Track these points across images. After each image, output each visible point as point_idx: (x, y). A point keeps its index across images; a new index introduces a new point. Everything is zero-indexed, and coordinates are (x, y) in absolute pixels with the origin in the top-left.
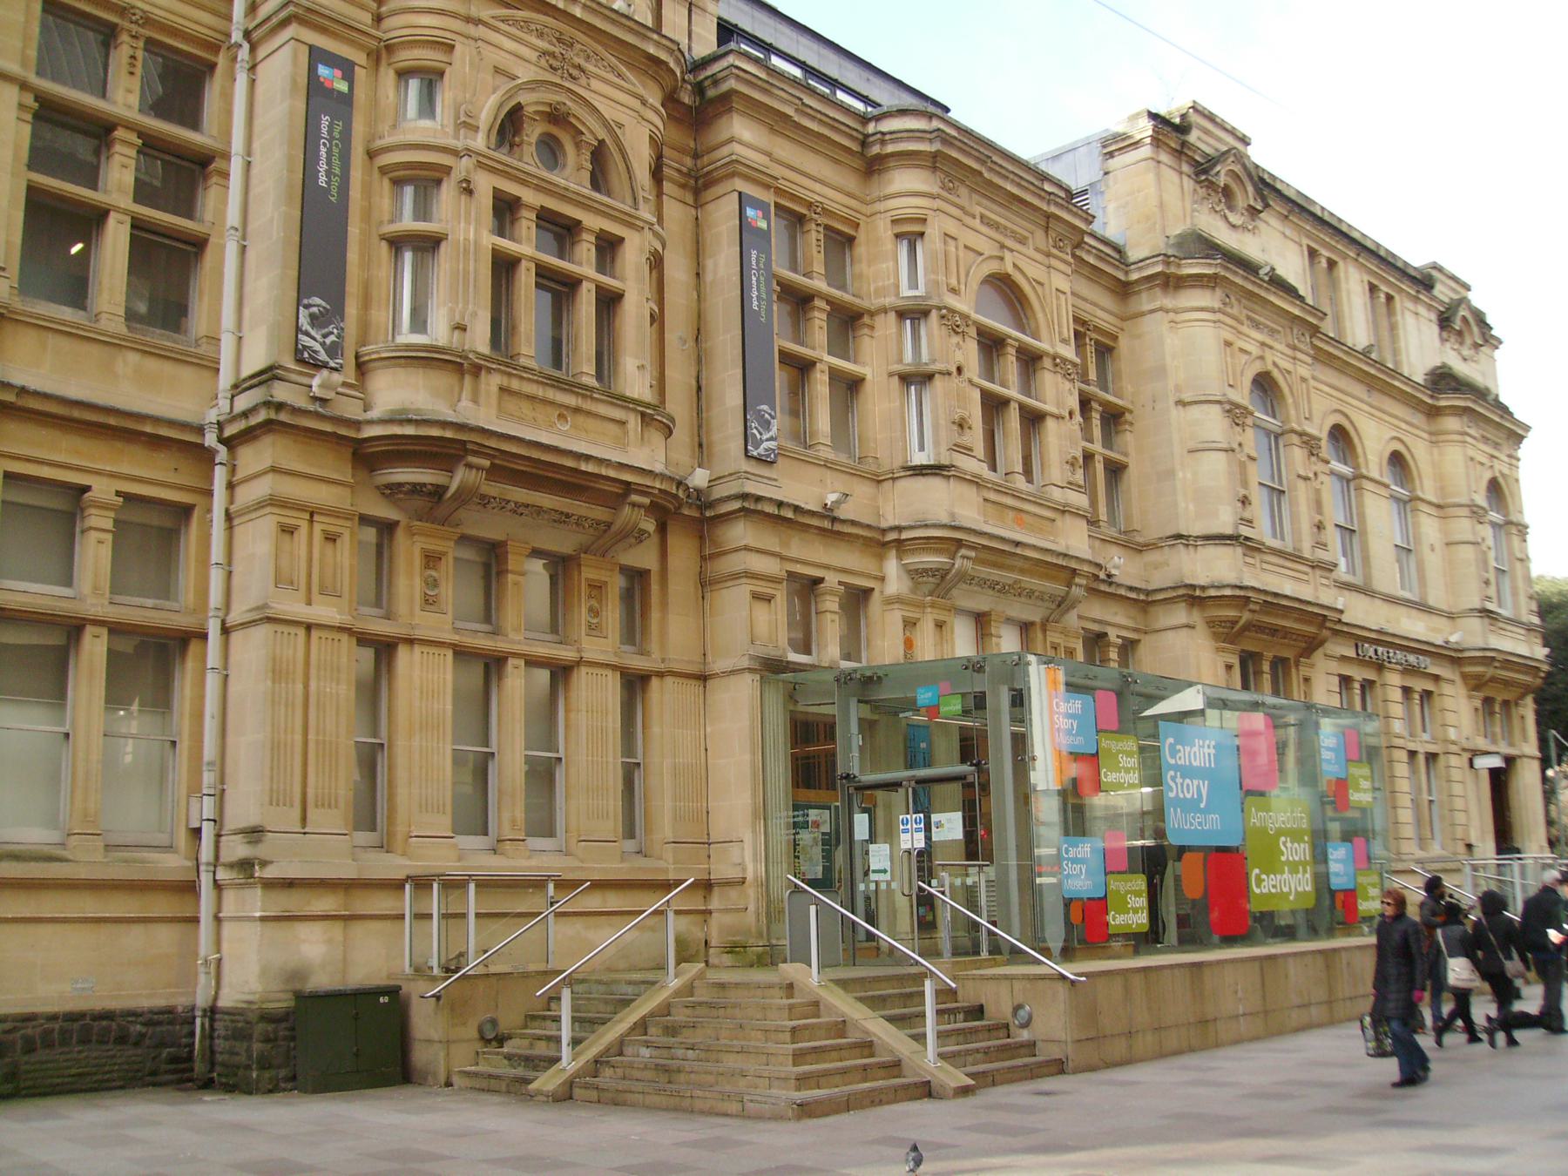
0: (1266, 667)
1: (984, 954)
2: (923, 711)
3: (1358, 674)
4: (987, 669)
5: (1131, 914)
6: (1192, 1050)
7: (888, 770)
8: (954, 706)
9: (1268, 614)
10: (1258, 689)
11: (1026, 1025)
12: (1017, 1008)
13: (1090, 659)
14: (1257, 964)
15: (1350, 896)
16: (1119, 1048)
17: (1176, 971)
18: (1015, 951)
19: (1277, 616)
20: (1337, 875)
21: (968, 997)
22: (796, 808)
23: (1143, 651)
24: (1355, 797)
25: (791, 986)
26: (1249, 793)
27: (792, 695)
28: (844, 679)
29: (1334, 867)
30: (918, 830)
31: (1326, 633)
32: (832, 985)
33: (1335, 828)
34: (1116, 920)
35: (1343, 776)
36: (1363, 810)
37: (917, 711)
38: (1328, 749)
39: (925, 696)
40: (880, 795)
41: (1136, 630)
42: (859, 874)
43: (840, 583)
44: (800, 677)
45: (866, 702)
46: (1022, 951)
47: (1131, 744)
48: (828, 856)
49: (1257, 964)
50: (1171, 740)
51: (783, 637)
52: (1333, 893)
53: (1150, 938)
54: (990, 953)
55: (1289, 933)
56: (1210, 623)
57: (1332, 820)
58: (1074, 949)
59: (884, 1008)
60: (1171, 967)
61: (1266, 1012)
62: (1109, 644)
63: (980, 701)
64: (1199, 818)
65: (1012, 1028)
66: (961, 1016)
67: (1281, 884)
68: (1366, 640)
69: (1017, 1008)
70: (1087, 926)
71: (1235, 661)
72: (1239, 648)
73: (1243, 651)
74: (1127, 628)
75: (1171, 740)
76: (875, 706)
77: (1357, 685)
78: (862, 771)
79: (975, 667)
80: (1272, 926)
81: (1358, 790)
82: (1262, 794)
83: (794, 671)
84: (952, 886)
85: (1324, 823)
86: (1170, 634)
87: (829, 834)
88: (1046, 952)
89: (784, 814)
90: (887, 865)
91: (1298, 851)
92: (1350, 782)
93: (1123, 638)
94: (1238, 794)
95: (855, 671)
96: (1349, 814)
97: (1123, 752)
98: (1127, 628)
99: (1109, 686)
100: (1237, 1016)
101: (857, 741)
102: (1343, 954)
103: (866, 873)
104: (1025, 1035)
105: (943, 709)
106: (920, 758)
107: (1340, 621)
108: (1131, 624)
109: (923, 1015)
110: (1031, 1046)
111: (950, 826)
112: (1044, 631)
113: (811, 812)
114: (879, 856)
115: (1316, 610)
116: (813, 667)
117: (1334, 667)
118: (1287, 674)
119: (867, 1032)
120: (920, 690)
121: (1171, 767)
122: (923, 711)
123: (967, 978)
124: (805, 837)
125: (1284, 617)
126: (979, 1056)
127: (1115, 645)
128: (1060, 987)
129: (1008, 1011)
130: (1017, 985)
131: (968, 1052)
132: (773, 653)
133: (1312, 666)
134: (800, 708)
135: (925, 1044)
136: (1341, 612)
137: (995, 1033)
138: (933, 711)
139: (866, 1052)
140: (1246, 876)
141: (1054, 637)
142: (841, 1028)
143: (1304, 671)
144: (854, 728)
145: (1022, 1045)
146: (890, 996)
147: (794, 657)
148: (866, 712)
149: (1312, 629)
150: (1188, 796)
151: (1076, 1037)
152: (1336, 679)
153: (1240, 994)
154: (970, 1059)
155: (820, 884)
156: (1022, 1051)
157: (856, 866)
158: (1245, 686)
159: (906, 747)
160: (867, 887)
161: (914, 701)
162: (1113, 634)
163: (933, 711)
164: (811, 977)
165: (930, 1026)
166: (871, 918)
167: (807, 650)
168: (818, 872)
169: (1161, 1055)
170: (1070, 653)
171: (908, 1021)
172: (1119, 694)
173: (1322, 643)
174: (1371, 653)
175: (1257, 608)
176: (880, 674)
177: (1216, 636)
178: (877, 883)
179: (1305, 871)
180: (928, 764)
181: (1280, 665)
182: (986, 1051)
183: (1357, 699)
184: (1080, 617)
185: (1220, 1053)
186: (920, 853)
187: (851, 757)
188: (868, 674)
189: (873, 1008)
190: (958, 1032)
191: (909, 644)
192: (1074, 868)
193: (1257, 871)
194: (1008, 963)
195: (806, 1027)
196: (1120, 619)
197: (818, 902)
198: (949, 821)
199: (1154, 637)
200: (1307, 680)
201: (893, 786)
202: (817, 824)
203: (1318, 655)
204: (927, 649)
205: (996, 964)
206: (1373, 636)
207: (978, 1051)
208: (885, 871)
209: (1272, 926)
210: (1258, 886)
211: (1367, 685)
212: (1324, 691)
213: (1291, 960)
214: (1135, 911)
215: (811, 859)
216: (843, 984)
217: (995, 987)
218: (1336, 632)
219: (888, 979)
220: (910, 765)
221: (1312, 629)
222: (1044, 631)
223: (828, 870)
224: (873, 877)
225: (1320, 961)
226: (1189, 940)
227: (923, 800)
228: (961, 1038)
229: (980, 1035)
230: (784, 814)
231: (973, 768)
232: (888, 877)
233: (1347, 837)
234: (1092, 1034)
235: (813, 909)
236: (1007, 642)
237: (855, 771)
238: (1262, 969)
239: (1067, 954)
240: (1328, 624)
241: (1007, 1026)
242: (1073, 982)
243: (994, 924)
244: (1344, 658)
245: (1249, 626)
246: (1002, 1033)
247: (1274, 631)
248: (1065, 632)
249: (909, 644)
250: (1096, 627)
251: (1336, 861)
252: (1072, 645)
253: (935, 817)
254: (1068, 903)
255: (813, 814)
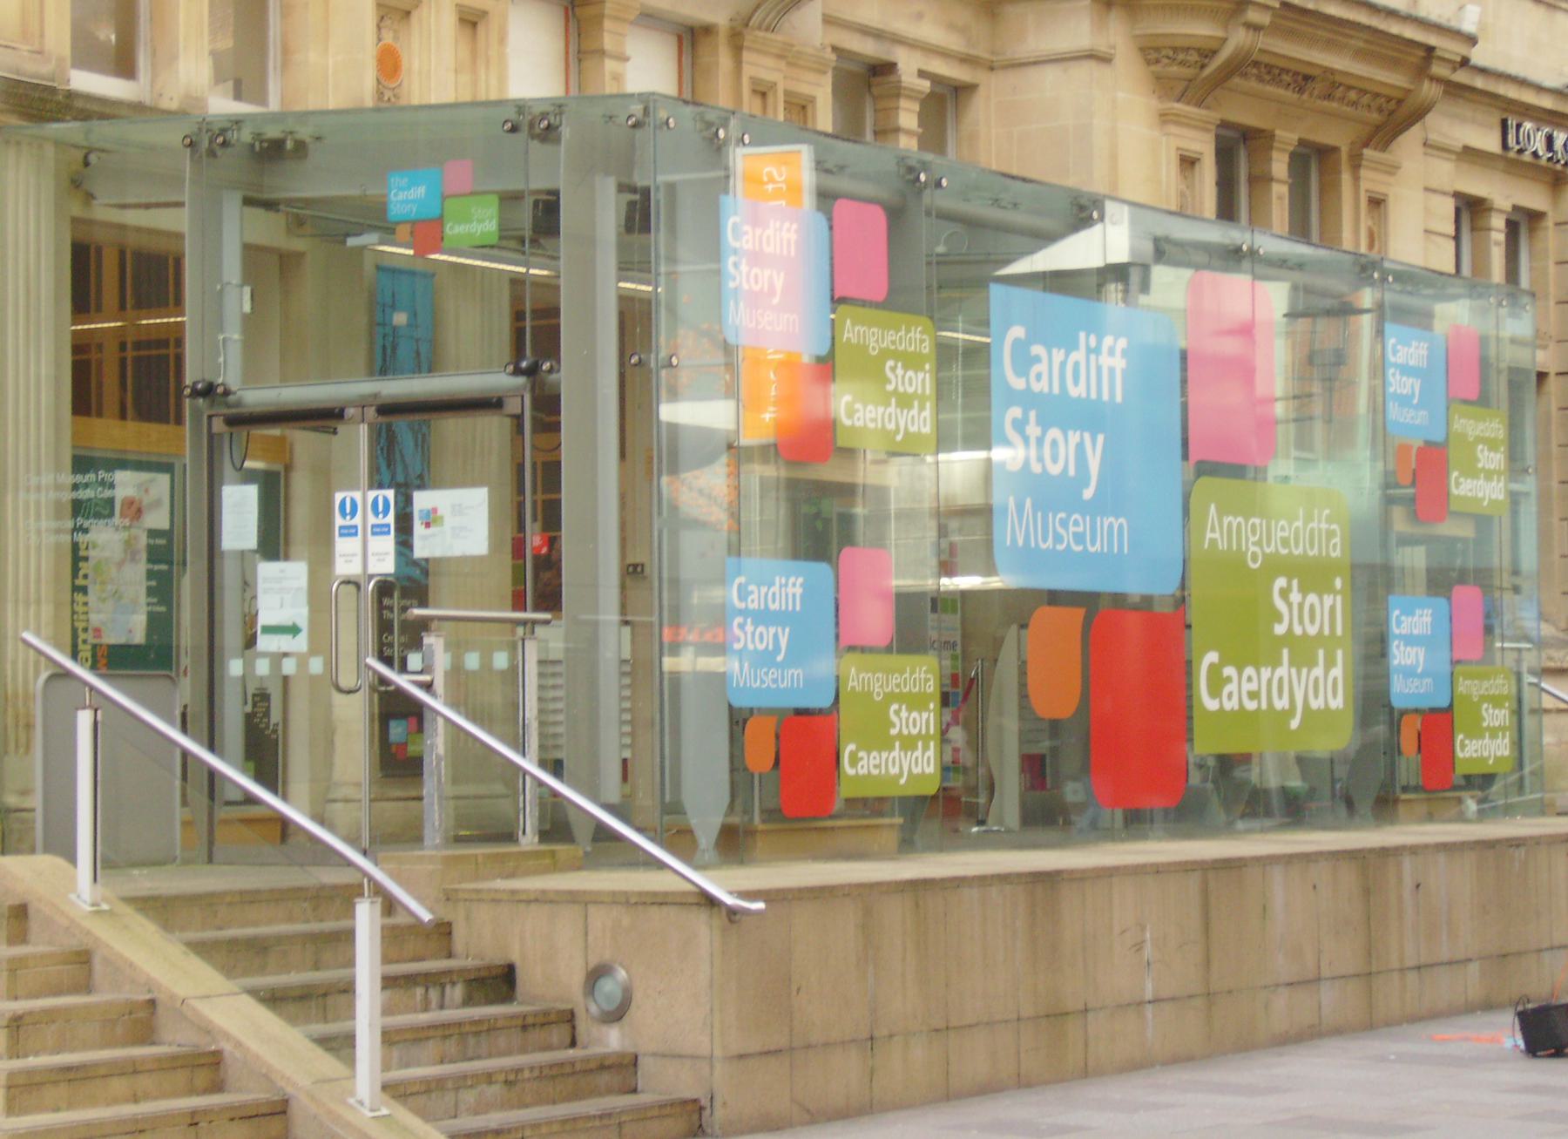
0: (1279, 166)
1: (529, 840)
2: (403, 232)
3: (1503, 193)
4: (566, 132)
5: (900, 749)
6: (1023, 1083)
7: (326, 376)
8: (483, 222)
9: (1290, 34)
10: (1259, 220)
11: (617, 1015)
12: (597, 974)
13: (850, 129)
14: (1194, 881)
15: (1438, 726)
16: (843, 1075)
17: (994, 891)
18: (603, 834)
19: (1313, 41)
20: (1409, 672)
21: (479, 943)
22: (82, 464)
23: (983, 113)
24: (1463, 487)
25: (20, 912)
26: (1206, 469)
27: (78, 180)
28: (210, 142)
29: (1402, 656)
30: (379, 530)
31: (1429, 90)
32: (128, 910)
33: (1415, 559)
34: (866, 766)
35: (1438, 436)
36: (1483, 521)
37: (388, 230)
38: (1405, 370)
39: (407, 196)
40: (303, 440)
41: (966, 60)
42: (231, 635)
43: (922, 74)
44: (103, 132)
45: (270, 205)
46: (617, 837)
47: (916, 337)
48: (162, 588)
49: (1194, 881)
50: (1017, 332)
51: (58, 37)
52: (1395, 718)
53: (949, 808)
54: (545, 836)
55: (1293, 810)
56: (1152, 52)
57: (1405, 541)
58: (751, 833)
59: (262, 970)
60: (983, 881)
61: (1209, 995)
62: (897, 92)
63: (547, 213)
64: (1079, 523)
65: (582, 1026)
66: (457, 992)
67: (1276, 692)
68: (1528, 111)
69: (597, 974)
70: (790, 774)
71: (1204, 147)
72: (1215, 116)
73: (1224, 124)
74: (944, 54)
75: (1017, 332)
76: (301, 216)
77: (1498, 222)
78: (252, 375)
79: (537, 126)
80: (1235, 791)
81: (1471, 472)
82: (1236, 471)
83: (84, 116)
84: (456, 672)
85: (1384, 545)
86: (1051, 74)
87: (167, 534)
88: (679, 839)
89: (47, 479)
90: (299, 613)
91: (1320, 613)
92: (1452, 454)
93: (935, 79)
94: (1174, 471)
95: (238, 122)
96: (1448, 529)
97: (897, 355)
98: (944, 54)
99: (868, 189)
100: (1140, 1004)
101: (240, 301)
102: (1407, 863)
103: (251, 642)
104: (613, 1040)
105: (453, 230)
106: (404, 352)
107: (1465, 62)
108: (954, 42)
109: (348, 989)
110: (625, 1068)
111: (461, 522)
112: (737, 47)
113: (121, 476)
114: (281, 591)
115: (1409, 32)
116: (138, 109)
117: (1449, 175)
118: (1330, 188)
119: (208, 1030)
120: (396, 180)
121: (1013, 397)
122: (403, 232)
123: (478, 897)
124: (105, 538)
125: (1330, 45)
126: (495, 1090)
127: (912, 94)
128: (702, 925)
129: (575, 979)
130: (599, 918)
131: (462, 1082)
132: (33, 69)
133: (1392, 169)
134: (102, 212)
135: (351, 1062)
136: (1472, 40)
137: (536, 1036)
138: (428, 232)
139: (202, 1078)
140: (1188, 669)
141: (759, 66)
142: (144, 1018)
143: (1371, 180)
144: (232, 265)
145: (604, 1065)
146: (280, 939)
147: (87, 82)
148: (267, 229)
149: (1396, 79)
150: (1055, 470)
151: (735, 1049)
152: (1449, 206)
153: (1148, 951)
154: (469, 1097)
155: (117, 660)
156: (604, 1079)
157: (224, 618)
158: (1227, 211)
159: (372, 324)
160: (249, 666)
161: (381, 208)
162: (909, 66)
163: (428, 232)
164: (72, 888)
165: (367, 1011)
166: (264, 754)
167: (124, 66)
168: (133, 627)
169: (948, 1094)
170: (800, 107)
171: (316, 1002)
172: (896, 215)
173: (1418, 115)
174: (1539, 144)
175: (1264, 18)
176: (304, 133)
177: (1162, 86)
178: (278, 658)
179: (1330, 663)
180: (428, 363)
181: (1314, 161)
182: (511, 1080)
183: (1497, 256)
184: (829, 20)
185: (1093, 1091)
186: (385, 588)
187: (220, 339)
188: (273, 132)
189: (229, 971)
190: (444, 1030)
191: (389, 64)
192: (755, 630)
193: (1212, 657)
194: (589, 862)
195: (50, 1015)
196: (931, 31)
197: (100, 703)
198: (458, 510)
199: (1012, 77)
200: (1377, 203)
201: (325, 417)
202: (135, 510)
203: (1410, 141)
204: (436, 74)
205: (556, 867)
206: (1547, 102)
207: (489, 1077)
208: (293, 630)
209: (1235, 791)
210: (1215, 692)
211: (1522, 223)
212: (1417, 231)
213: (1277, 873)
214: (909, 743)
215: (117, 596)
216: (160, 908)
217: (545, 927)
218: (1456, 91)
219: (280, 896)
220: (384, 366)
221: (1396, 79)
222: (737, 47)
223: (161, 625)
224: (265, 643)
225: (1349, 876)
226: (1045, 816)
227: (405, 446)
228: (451, 1046)
229: (502, 1041)
230: (47, 479)
231: (520, 373)
232: (300, 643)
233: (1440, 582)
234: (780, 1040)
235: (84, 719)
236: (643, 68)
237: (230, 374)
238: (1205, 892)
239: (734, 843)
240: (1438, 69)
241: (570, 1018)
242: (732, 912)
243: (556, 768)
244: (1470, 155)
245: (1240, 65)
246: (558, 1034)
247: (1303, 79)
248: (788, 56)
249: (389, 64)
250: (869, 48)
251: (1410, 640)
252: (804, 89)
253: (422, 500)
254: (738, 720)
255: (126, 484)
